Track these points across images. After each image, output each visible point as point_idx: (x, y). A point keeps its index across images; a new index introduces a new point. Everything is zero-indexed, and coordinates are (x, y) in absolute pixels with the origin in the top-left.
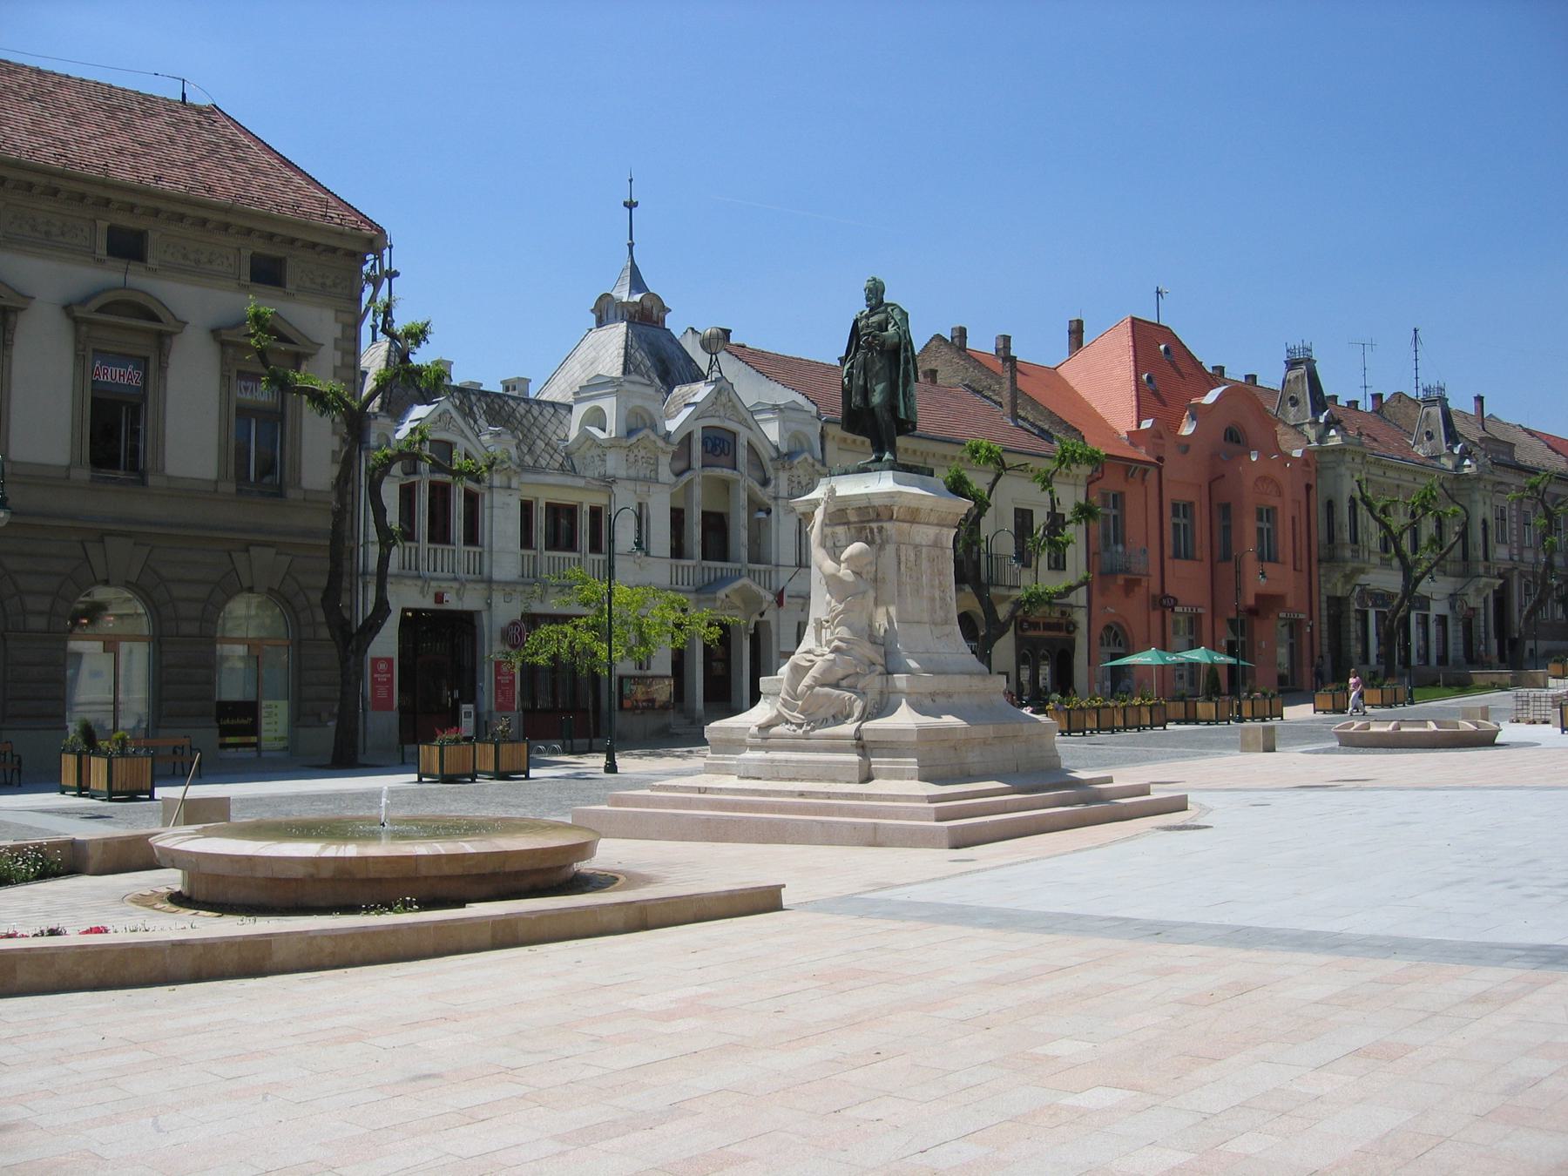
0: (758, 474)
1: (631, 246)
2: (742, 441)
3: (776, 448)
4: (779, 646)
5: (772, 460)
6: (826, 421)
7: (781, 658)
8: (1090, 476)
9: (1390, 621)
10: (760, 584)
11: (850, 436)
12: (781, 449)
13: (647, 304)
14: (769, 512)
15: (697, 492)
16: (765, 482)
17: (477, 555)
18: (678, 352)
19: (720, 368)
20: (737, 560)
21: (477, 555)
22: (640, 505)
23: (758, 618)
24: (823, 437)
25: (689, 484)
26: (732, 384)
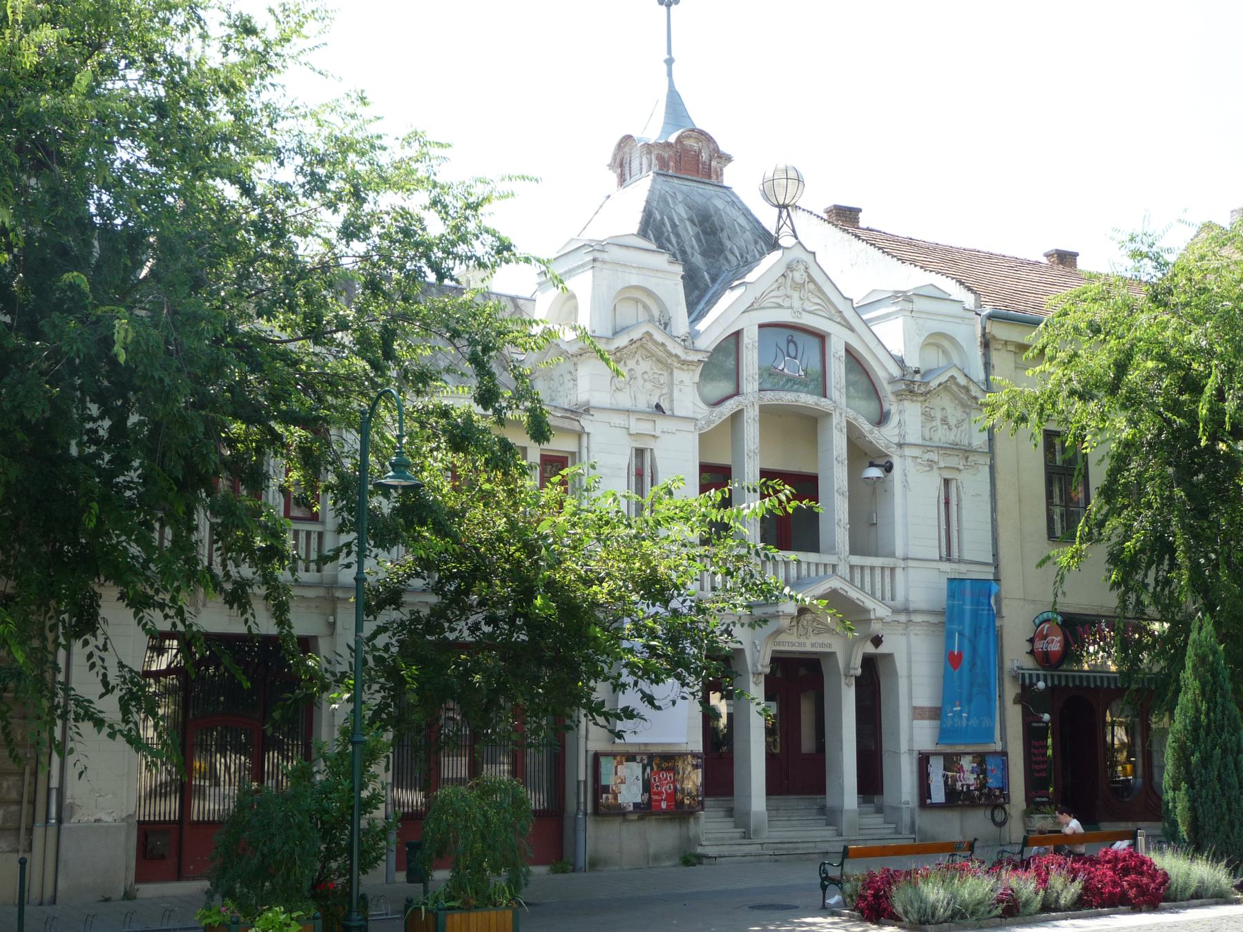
0: (871, 407)
1: (669, 62)
2: (836, 348)
3: (900, 362)
4: (910, 698)
5: (892, 381)
6: (990, 317)
7: (915, 718)
8: (674, 255)
9: (126, 19)
10: (862, 588)
11: (759, 519)
12: (908, 363)
13: (692, 143)
14: (888, 468)
15: (751, 431)
16: (882, 419)
17: (314, 538)
18: (742, 221)
19: (794, 231)
20: (832, 550)
21: (314, 538)
22: (640, 453)
23: (870, 649)
24: (986, 344)
25: (736, 417)
26: (814, 253)
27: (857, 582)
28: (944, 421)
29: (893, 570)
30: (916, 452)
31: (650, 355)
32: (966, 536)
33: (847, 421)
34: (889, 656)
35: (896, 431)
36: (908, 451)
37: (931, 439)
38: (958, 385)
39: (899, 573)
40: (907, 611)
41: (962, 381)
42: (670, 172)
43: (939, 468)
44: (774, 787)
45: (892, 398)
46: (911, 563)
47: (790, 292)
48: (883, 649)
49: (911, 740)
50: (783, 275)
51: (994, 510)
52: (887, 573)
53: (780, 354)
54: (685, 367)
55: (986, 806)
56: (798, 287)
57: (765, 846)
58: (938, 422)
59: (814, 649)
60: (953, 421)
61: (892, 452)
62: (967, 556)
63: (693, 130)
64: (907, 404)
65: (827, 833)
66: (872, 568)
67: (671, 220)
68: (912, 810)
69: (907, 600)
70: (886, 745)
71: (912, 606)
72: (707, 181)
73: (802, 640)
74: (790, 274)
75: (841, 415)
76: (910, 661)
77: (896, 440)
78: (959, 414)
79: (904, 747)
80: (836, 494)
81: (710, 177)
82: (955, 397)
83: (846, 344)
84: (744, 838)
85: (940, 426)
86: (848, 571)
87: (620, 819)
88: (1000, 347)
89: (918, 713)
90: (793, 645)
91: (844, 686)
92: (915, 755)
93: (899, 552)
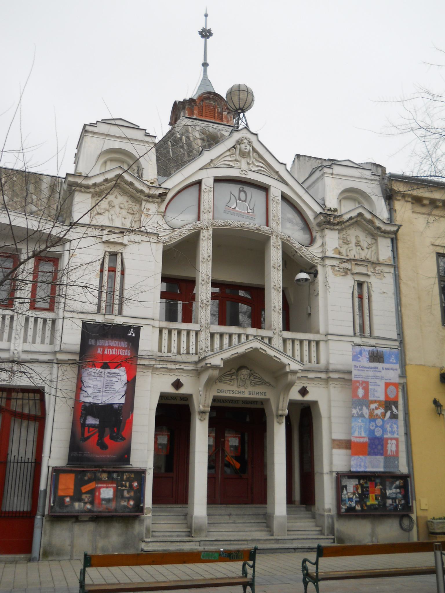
4: (331, 433)
5: (317, 216)
7: (333, 448)
14: (316, 274)
27: (290, 353)
28: (357, 244)
29: (318, 343)
30: (335, 263)
31: (125, 192)
32: (376, 320)
33: (283, 243)
34: (315, 403)
35: (320, 250)
36: (328, 262)
37: (347, 256)
38: (365, 219)
39: (322, 345)
40: (327, 371)
41: (368, 216)
42: (195, 117)
43: (353, 274)
44: (156, 500)
45: (316, 228)
46: (330, 337)
47: (238, 158)
48: (308, 398)
49: (331, 463)
50: (234, 147)
51: (399, 303)
52: (313, 344)
53: (233, 198)
54: (150, 200)
55: (395, 516)
56: (243, 154)
57: (202, 543)
58: (352, 245)
59: (251, 396)
60: (364, 245)
61: (316, 263)
62: (376, 333)
63: (210, 93)
64: (327, 231)
65: (262, 535)
66: (301, 342)
67: (188, 138)
68: (332, 517)
69: (328, 363)
70: (317, 469)
71: (331, 367)
72: (220, 122)
73: (242, 389)
74: (238, 146)
75: (277, 236)
76: (330, 407)
77: (320, 255)
78: (369, 240)
79: (326, 469)
80: (272, 290)
81: (222, 121)
82: (365, 230)
83: (282, 192)
84: (189, 536)
85: (354, 247)
86: (282, 344)
87: (74, 520)
88: (400, 198)
89: (337, 444)
90: (234, 392)
91: (276, 425)
92: (334, 475)
93: (322, 330)
